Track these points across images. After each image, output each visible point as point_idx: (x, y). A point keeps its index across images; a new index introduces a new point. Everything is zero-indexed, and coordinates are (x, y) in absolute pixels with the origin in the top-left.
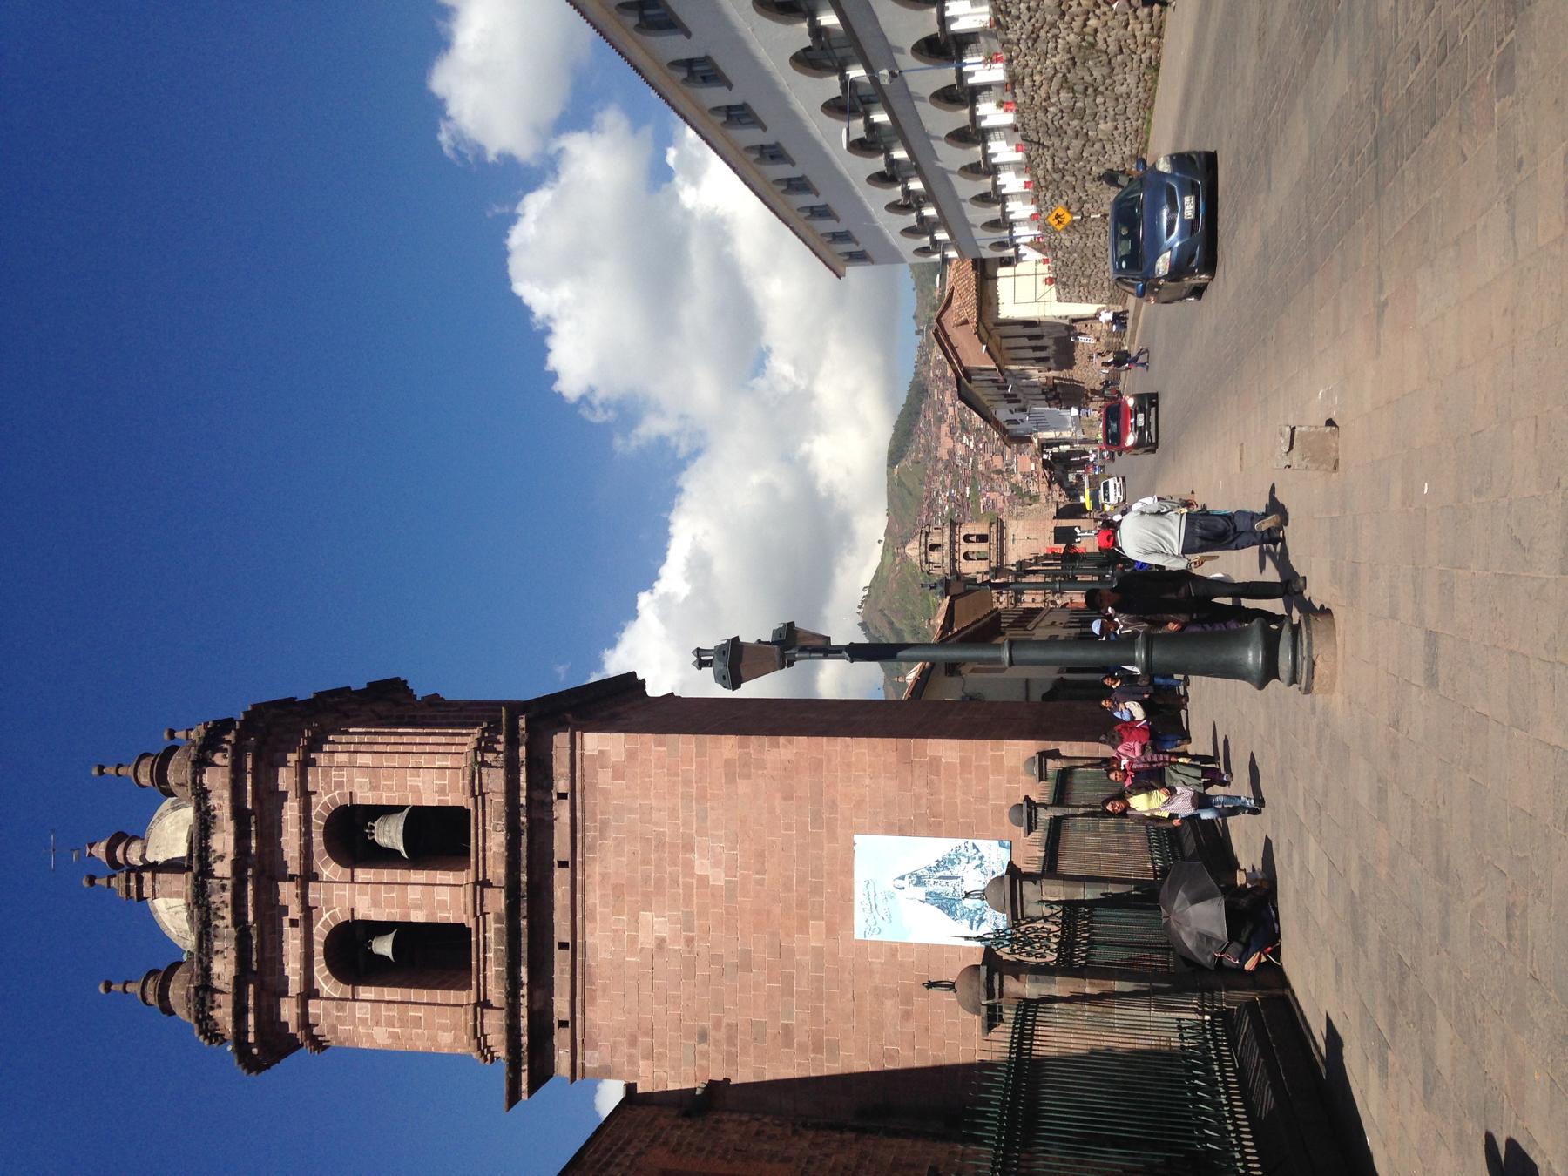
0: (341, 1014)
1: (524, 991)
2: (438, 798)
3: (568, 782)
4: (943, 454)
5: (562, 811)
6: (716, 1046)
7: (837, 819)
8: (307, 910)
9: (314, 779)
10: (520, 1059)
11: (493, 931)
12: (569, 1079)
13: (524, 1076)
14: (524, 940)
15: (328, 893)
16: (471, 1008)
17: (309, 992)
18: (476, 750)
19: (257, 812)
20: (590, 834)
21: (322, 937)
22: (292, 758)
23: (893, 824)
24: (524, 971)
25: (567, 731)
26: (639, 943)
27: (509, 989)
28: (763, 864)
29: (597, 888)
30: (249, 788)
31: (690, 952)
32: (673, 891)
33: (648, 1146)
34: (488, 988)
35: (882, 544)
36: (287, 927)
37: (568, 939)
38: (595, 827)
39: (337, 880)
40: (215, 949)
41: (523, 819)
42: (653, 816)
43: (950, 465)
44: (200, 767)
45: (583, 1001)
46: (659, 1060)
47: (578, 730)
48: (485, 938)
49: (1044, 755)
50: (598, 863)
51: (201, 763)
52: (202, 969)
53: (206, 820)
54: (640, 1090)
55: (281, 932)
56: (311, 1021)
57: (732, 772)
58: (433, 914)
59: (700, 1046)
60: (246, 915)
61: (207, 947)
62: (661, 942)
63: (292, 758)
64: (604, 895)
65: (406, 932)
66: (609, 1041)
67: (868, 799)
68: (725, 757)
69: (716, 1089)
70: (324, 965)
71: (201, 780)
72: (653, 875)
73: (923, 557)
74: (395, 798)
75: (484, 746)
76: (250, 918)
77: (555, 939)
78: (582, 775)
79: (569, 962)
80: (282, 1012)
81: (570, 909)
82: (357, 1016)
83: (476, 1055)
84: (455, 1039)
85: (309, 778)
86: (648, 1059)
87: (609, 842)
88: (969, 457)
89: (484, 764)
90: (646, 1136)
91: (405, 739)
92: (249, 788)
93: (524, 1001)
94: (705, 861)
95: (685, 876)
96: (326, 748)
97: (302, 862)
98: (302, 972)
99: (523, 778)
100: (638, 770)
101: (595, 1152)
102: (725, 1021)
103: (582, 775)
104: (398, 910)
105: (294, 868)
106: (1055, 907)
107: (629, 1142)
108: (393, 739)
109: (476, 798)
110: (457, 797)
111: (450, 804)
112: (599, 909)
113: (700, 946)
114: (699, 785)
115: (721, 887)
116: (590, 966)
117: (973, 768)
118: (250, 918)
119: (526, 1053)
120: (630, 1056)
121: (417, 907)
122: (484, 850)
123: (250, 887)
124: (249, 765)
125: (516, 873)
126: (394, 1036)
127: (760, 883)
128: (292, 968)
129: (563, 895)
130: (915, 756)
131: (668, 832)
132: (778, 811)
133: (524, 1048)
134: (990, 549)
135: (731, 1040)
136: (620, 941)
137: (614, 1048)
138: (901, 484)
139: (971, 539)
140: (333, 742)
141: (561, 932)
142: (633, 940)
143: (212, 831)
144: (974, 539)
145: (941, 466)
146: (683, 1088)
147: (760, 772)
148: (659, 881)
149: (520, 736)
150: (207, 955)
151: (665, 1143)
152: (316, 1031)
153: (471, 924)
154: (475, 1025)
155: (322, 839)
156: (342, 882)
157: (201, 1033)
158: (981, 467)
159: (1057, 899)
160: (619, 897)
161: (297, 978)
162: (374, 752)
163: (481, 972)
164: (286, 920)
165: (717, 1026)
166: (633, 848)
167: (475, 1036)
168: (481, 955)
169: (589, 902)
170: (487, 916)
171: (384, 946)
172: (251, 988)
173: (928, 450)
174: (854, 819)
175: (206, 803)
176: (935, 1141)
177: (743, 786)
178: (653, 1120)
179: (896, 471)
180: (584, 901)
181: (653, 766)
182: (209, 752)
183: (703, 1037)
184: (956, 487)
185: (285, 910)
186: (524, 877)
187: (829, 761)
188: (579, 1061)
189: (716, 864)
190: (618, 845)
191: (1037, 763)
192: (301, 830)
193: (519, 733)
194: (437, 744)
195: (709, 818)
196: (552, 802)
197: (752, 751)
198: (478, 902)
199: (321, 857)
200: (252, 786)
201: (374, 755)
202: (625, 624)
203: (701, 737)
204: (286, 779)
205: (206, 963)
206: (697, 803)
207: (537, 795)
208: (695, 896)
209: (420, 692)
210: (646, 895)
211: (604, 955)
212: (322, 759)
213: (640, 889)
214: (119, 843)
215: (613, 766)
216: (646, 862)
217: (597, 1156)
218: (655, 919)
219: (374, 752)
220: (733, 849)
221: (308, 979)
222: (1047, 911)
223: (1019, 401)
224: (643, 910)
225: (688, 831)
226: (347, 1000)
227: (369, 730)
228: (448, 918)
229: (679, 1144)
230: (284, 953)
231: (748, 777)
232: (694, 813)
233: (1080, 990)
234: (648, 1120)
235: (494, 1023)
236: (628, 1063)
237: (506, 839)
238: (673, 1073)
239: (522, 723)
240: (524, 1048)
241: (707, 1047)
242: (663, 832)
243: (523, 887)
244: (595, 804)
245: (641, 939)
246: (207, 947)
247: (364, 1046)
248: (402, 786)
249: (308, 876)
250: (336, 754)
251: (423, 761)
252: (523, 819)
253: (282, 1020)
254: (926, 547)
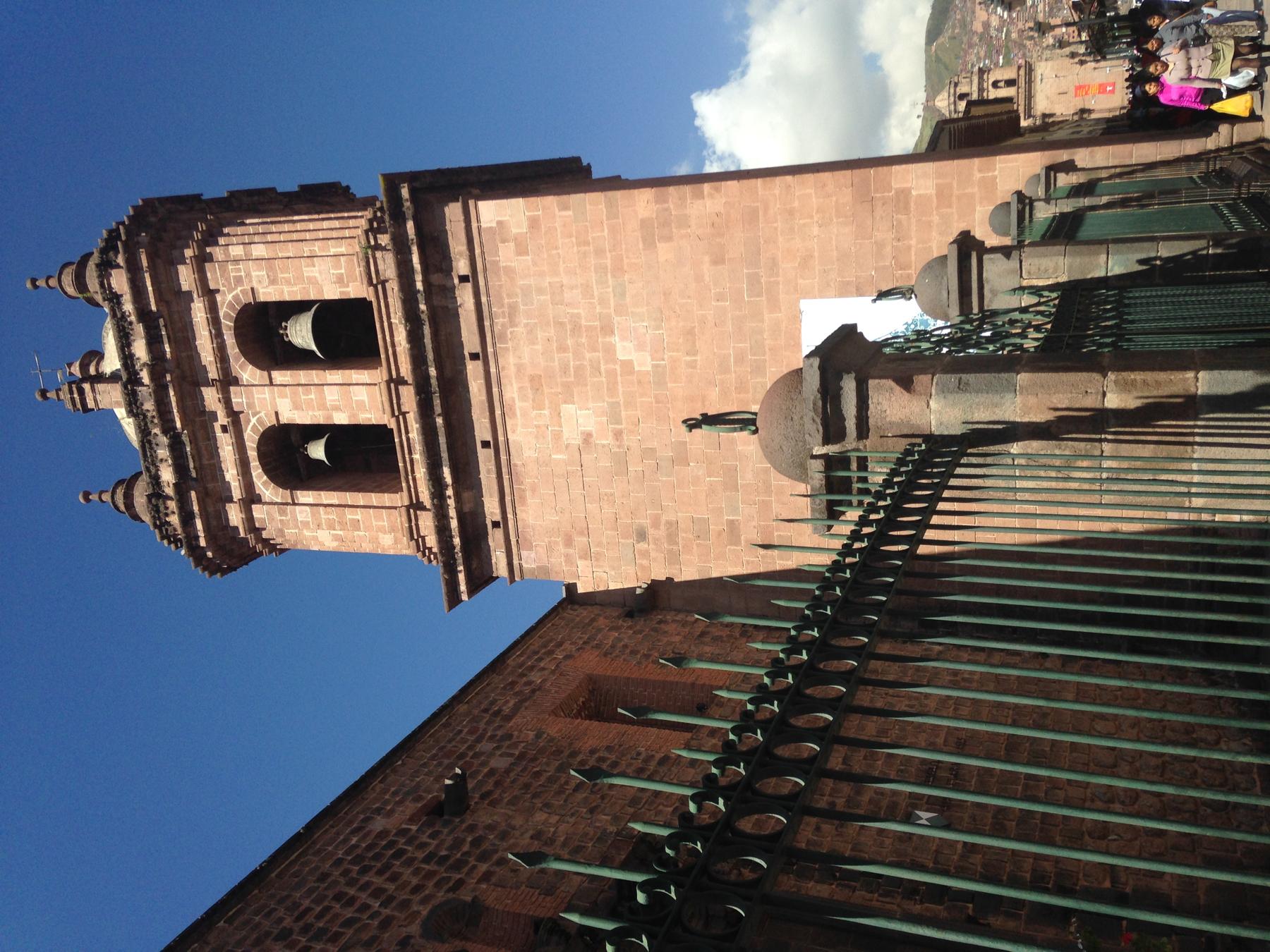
0: (284, 518)
1: (450, 492)
2: (339, 290)
3: (467, 262)
4: (978, 27)
5: (465, 296)
6: (656, 544)
7: (778, 283)
8: (234, 415)
9: (214, 277)
10: (455, 560)
11: (415, 431)
12: (508, 580)
13: (462, 577)
14: (442, 440)
15: (248, 397)
16: (403, 510)
17: (251, 498)
18: (366, 232)
19: (165, 313)
20: (499, 321)
21: (253, 442)
22: (188, 253)
23: (848, 283)
24: (447, 472)
25: (458, 201)
26: (565, 438)
27: (433, 490)
28: (694, 343)
29: (514, 381)
30: (150, 289)
31: (619, 447)
32: (595, 379)
33: (578, 649)
34: (420, 490)
35: (921, 119)
36: (219, 433)
37: (489, 438)
38: (503, 312)
39: (257, 383)
40: (160, 457)
41: (423, 307)
42: (565, 295)
43: (985, 37)
44: (106, 270)
45: (513, 502)
46: (597, 560)
47: (472, 198)
48: (408, 439)
49: (1052, 169)
50: (511, 353)
51: (106, 267)
52: (150, 476)
53: (124, 328)
54: (580, 590)
55: (215, 438)
56: (257, 525)
57: (651, 234)
58: (354, 416)
59: (639, 545)
60: (173, 421)
61: (151, 455)
62: (587, 437)
63: (188, 253)
64: (522, 387)
65: (340, 437)
66: (544, 542)
67: (816, 254)
68: (640, 217)
69: (655, 588)
70: (260, 470)
71: (109, 284)
72: (572, 363)
73: (952, 107)
74: (296, 292)
75: (374, 229)
76: (178, 425)
77: (477, 438)
78: (483, 253)
79: (493, 462)
80: (230, 517)
81: (487, 405)
82: (299, 519)
83: (419, 555)
84: (395, 541)
85: (209, 275)
86: (586, 559)
87: (520, 330)
88: (1002, 28)
89: (377, 247)
90: (581, 638)
91: (299, 226)
92: (150, 289)
93: (451, 502)
94: (626, 344)
95: (607, 362)
96: (222, 241)
97: (219, 365)
98: (240, 478)
99: (416, 259)
100: (543, 242)
101: (521, 655)
102: (664, 519)
103: (483, 253)
104: (321, 412)
105: (213, 374)
106: (1046, 293)
107: (560, 644)
108: (286, 227)
109: (375, 287)
110: (357, 289)
111: (352, 296)
112: (518, 404)
113: (630, 440)
114: (614, 253)
115: (648, 372)
116: (516, 465)
117: (954, 198)
118: (178, 425)
119: (460, 554)
120: (567, 556)
121: (337, 408)
122: (393, 345)
123: (172, 393)
124: (145, 263)
125: (423, 368)
126: (336, 538)
127: (692, 365)
128: (231, 474)
129: (479, 390)
130: (876, 191)
131: (583, 314)
132: (707, 278)
133: (458, 549)
134: (1018, 93)
135: (672, 537)
136: (544, 438)
137: (550, 548)
138: (938, 60)
139: (999, 85)
140: (228, 235)
141: (482, 431)
142: (557, 436)
143: (132, 338)
144: (1002, 84)
145: (976, 39)
146: (626, 587)
147: (683, 232)
148: (579, 370)
149: (404, 209)
150: (154, 464)
151: (598, 646)
152: (265, 535)
153: (392, 424)
154: (410, 527)
155: (234, 341)
156: (262, 385)
157: (163, 538)
158: (1014, 36)
159: (1050, 282)
160: (538, 389)
161: (237, 484)
162: (268, 242)
163: (410, 474)
164: (217, 427)
165: (656, 524)
166: (547, 334)
167: (412, 538)
168: (407, 456)
169: (507, 396)
170: (407, 415)
171: (317, 451)
172: (193, 494)
173: (964, 25)
174: (800, 281)
175: (120, 309)
176: (905, 642)
177: (664, 251)
178: (593, 620)
179: (933, 48)
180: (501, 395)
181: (559, 236)
182: (111, 254)
183: (642, 535)
184: (990, 58)
185: (213, 416)
186: (433, 372)
187: (766, 209)
188: (516, 562)
189: (640, 347)
190: (530, 332)
191: (1043, 179)
192: (211, 333)
193: (403, 206)
194: (332, 229)
195: (628, 293)
196: (454, 287)
197: (672, 207)
198: (395, 401)
199: (237, 360)
200: (152, 286)
201: (267, 245)
203: (610, 194)
204: (186, 277)
205: (153, 471)
206: (614, 276)
207: (436, 278)
208: (620, 384)
210: (567, 387)
211: (529, 453)
212: (217, 252)
213: (559, 380)
214: (91, 362)
215: (516, 239)
216: (563, 348)
217: (522, 659)
218: (578, 412)
219: (268, 242)
220: (658, 328)
221: (248, 485)
222: (1027, 300)
224: (565, 402)
225: (605, 311)
226: (287, 504)
227: (265, 220)
228: (370, 419)
229: (613, 646)
230: (221, 459)
231: (669, 239)
232: (611, 289)
233: (1091, 402)
234: (587, 621)
235: (427, 523)
236: (566, 561)
237: (406, 329)
238: (613, 573)
239: (405, 192)
240: (458, 549)
241: (646, 546)
242: (579, 314)
243: (434, 382)
244: (500, 286)
245: (566, 434)
246: (151, 455)
247: (316, 548)
248: (300, 278)
249: (228, 381)
250: (230, 247)
251: (316, 249)
252: (423, 307)
253: (231, 525)
254: (955, 97)
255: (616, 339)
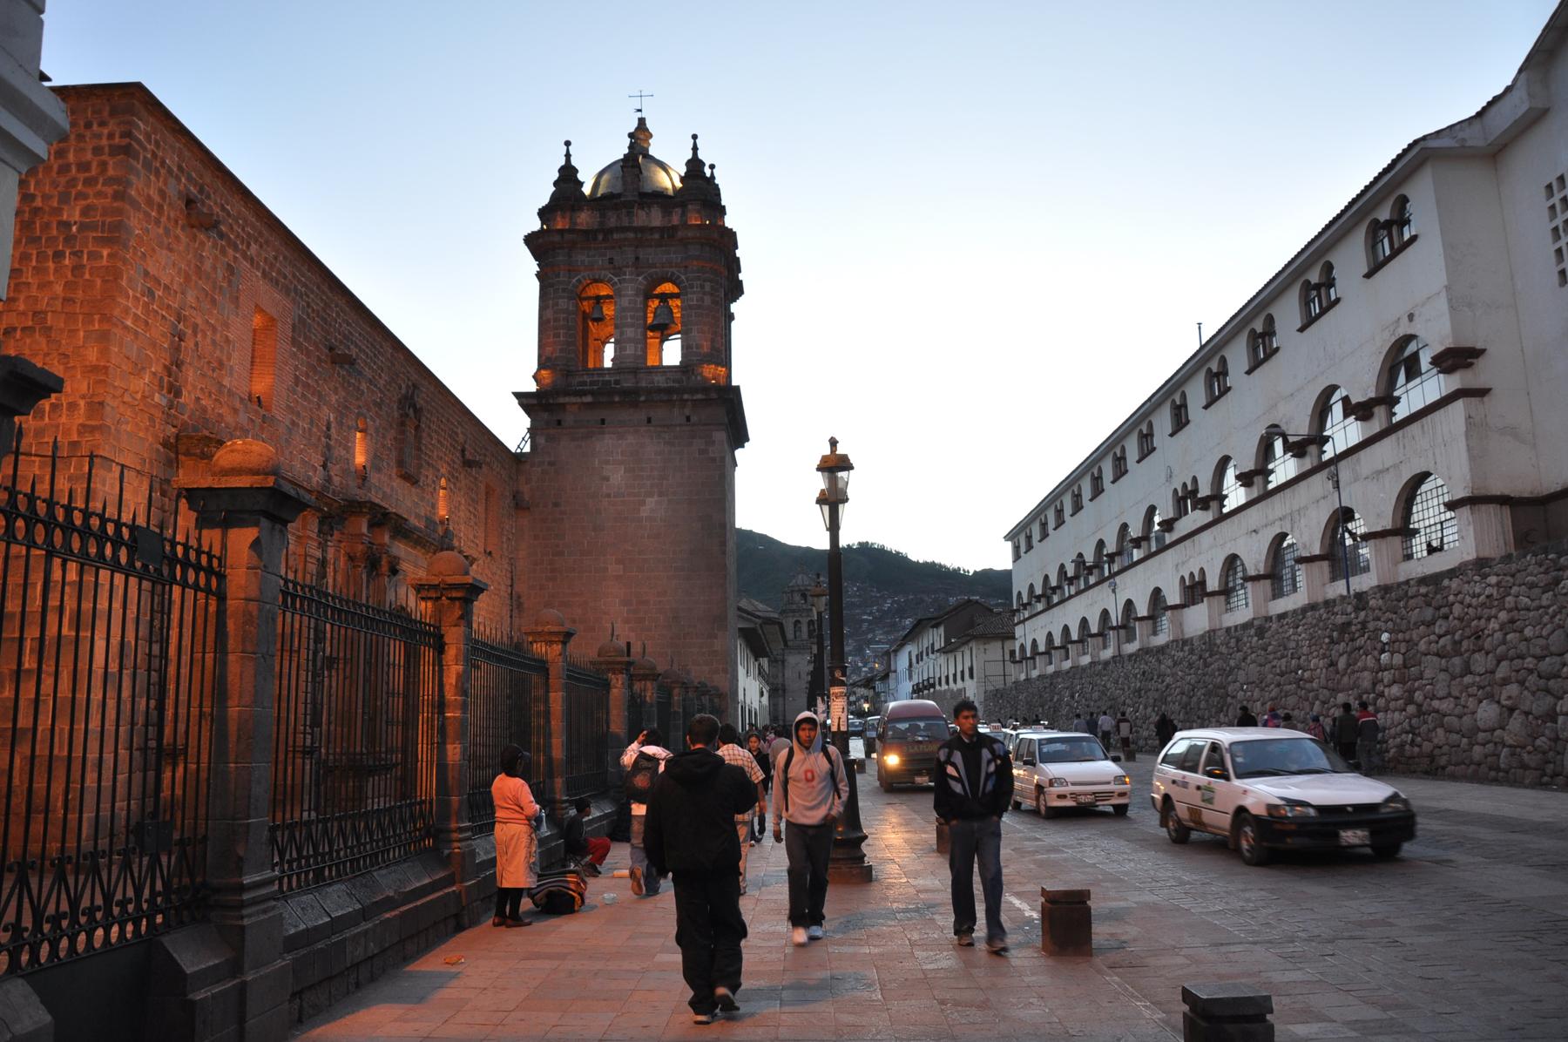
62: (607, 479)
142: (607, 462)
202: (645, 145)
209: (734, 307)
223: (918, 663)
255: (656, 498)
